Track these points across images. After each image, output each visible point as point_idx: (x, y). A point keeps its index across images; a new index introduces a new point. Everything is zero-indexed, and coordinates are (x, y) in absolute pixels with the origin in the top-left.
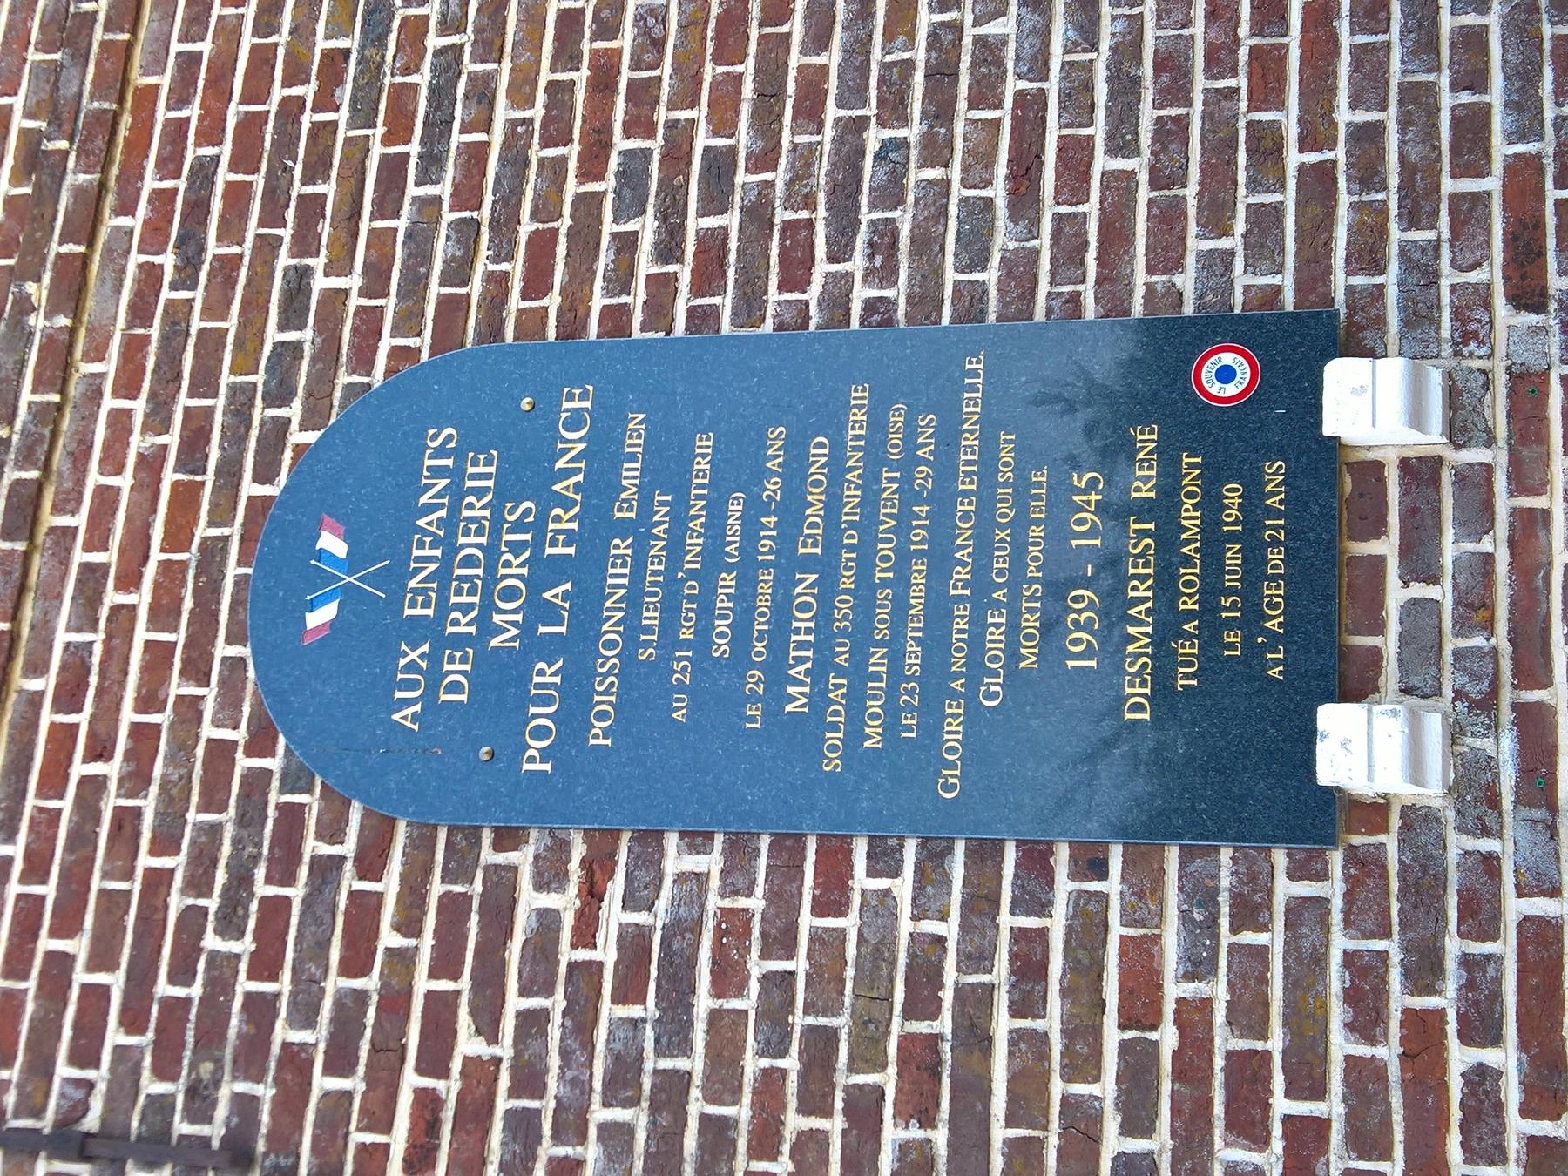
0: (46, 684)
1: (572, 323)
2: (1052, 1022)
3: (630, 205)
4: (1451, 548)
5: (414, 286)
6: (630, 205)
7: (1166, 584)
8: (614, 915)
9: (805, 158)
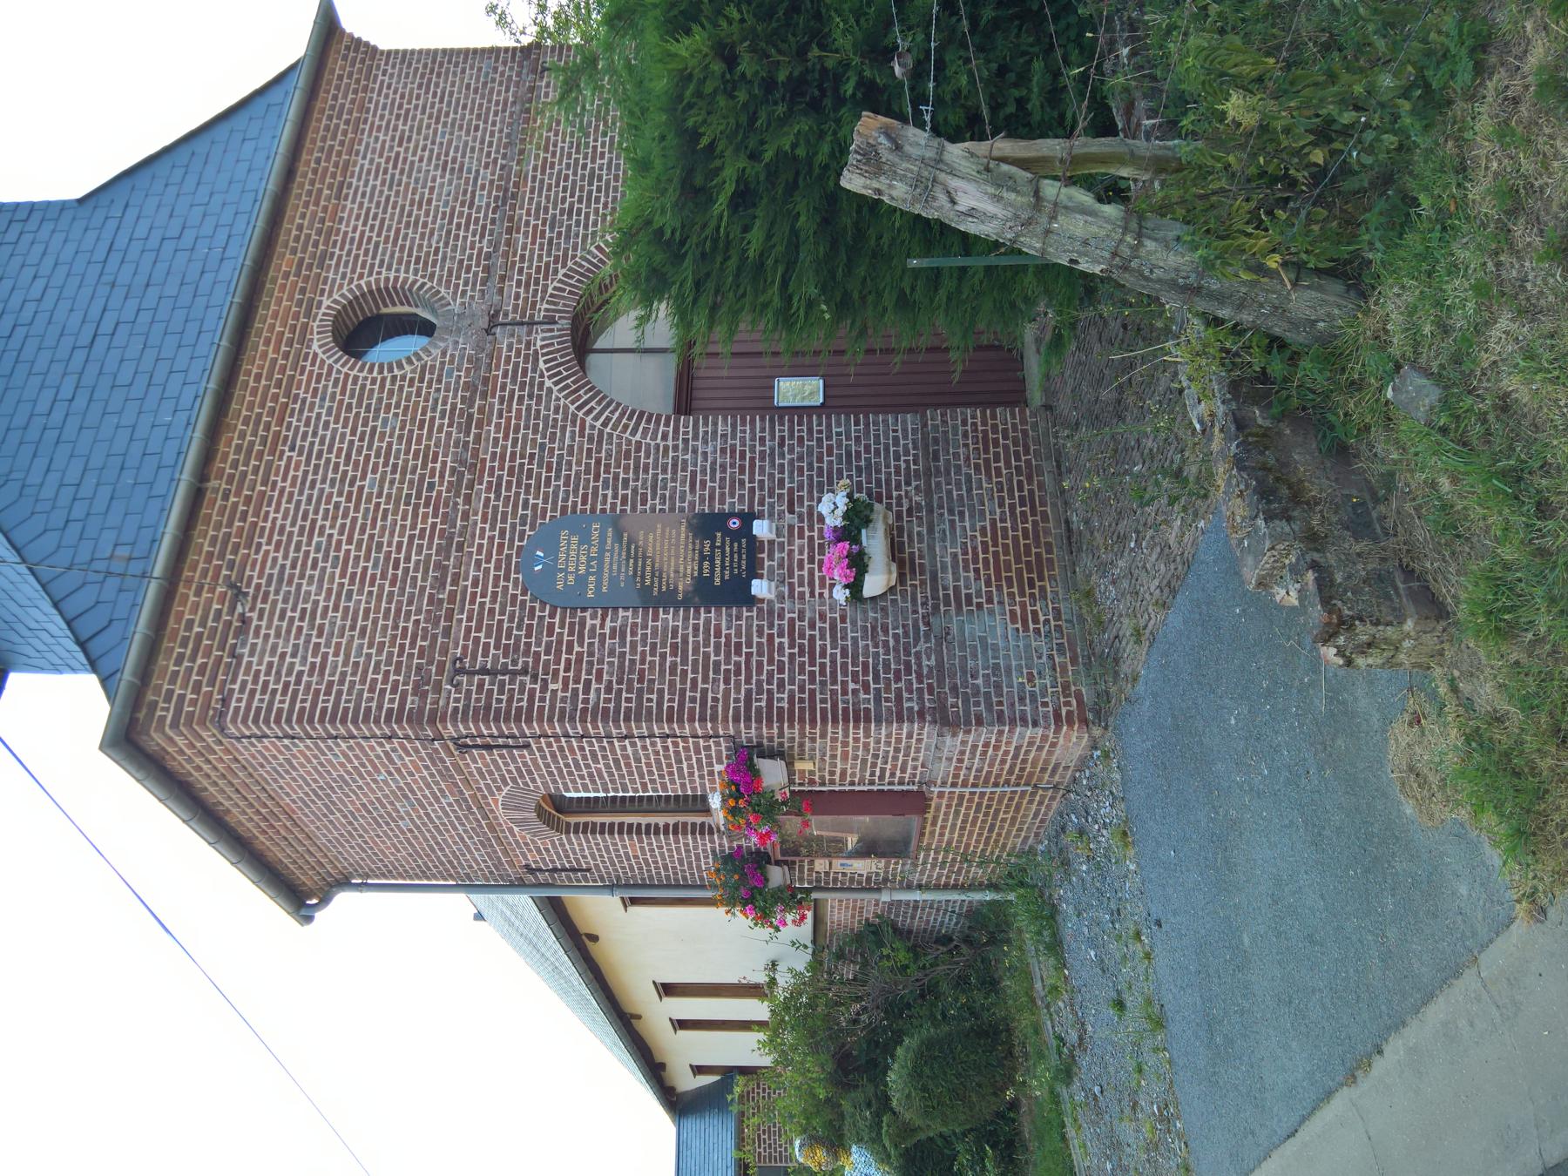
0: (469, 583)
1: (593, 510)
2: (701, 638)
3: (606, 487)
4: (777, 555)
5: (555, 503)
6: (606, 487)
7: (723, 562)
8: (608, 624)
9: (645, 481)
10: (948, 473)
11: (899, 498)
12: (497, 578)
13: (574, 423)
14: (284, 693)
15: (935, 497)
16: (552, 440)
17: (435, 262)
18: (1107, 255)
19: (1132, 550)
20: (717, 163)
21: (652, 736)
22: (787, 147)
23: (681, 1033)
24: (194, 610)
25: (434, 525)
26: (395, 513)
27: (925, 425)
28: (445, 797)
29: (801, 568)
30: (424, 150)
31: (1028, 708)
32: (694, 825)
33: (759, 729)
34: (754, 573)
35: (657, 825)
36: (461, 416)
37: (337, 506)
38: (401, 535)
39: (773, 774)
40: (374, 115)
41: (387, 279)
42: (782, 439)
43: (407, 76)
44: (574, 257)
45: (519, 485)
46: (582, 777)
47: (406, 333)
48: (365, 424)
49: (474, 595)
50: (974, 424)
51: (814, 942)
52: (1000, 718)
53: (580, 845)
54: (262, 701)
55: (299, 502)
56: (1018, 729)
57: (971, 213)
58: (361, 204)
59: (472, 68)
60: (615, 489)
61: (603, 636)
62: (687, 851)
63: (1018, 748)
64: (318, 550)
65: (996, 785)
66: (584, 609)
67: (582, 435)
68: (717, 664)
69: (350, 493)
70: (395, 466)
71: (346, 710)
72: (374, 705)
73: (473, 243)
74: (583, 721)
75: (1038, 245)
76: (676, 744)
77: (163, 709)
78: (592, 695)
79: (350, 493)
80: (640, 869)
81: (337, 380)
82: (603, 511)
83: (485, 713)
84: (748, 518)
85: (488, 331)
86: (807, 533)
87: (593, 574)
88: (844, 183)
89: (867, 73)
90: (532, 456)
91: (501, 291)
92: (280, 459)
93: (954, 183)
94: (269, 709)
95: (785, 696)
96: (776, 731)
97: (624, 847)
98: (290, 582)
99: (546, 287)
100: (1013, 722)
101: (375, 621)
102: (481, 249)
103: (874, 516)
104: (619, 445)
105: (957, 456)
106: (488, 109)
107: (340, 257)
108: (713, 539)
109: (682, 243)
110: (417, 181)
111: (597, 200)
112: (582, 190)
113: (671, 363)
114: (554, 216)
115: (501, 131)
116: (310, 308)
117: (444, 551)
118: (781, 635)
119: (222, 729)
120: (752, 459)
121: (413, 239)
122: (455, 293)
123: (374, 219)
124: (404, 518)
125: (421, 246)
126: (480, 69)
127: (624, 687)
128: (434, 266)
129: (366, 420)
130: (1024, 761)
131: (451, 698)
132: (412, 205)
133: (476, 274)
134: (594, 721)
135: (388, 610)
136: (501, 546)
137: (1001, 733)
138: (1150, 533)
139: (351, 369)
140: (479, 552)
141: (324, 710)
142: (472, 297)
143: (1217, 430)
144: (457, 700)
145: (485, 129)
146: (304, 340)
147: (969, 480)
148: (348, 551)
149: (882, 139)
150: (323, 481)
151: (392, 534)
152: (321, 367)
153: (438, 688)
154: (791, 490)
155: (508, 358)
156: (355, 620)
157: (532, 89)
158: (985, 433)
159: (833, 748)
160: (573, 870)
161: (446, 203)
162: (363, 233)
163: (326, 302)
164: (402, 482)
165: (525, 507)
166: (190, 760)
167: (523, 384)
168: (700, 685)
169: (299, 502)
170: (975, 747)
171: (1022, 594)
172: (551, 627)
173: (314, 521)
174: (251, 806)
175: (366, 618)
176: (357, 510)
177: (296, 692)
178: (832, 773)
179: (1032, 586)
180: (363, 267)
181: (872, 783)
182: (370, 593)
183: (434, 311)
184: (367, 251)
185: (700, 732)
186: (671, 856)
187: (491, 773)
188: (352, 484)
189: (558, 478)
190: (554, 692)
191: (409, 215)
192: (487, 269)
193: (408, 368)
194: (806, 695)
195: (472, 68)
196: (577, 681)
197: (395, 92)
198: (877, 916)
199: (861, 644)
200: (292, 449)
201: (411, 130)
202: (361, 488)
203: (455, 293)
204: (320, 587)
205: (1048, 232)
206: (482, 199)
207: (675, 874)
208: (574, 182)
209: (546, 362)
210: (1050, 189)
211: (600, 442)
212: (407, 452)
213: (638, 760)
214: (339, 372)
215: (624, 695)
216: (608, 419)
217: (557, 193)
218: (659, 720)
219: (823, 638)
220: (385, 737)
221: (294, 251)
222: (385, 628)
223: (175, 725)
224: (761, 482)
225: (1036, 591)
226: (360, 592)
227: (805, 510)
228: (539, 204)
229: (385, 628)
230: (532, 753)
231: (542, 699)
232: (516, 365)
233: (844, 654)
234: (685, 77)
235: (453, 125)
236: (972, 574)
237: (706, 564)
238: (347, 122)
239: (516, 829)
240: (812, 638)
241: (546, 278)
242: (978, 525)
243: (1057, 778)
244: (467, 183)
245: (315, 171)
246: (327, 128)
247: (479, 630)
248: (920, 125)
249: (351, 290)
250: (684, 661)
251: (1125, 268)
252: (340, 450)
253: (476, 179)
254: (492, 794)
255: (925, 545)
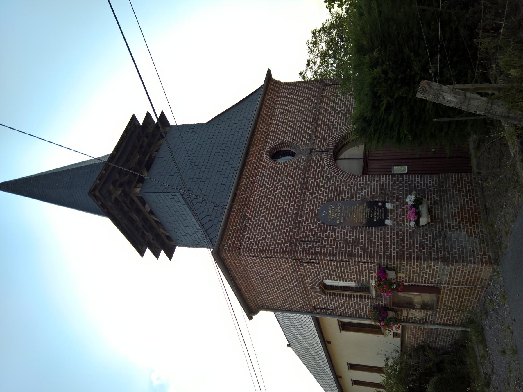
1: (339, 200)
2: (370, 235)
5: (328, 198)
10: (447, 191)
11: (431, 198)
12: (312, 217)
13: (333, 177)
14: (256, 244)
15: (442, 198)
16: (327, 182)
17: (296, 136)
18: (484, 109)
19: (505, 208)
20: (382, 99)
21: (355, 262)
22: (401, 94)
23: (355, 386)
24: (234, 223)
25: (295, 203)
26: (285, 200)
27: (439, 178)
28: (294, 279)
29: (400, 217)
30: (293, 107)
31: (472, 259)
32: (365, 296)
33: (387, 261)
34: (386, 217)
35: (354, 295)
36: (302, 175)
37: (270, 198)
38: (286, 206)
39: (391, 275)
40: (280, 99)
41: (283, 141)
42: (395, 181)
43: (289, 89)
44: (334, 134)
45: (318, 193)
46: (333, 275)
47: (287, 156)
48: (277, 177)
49: (305, 221)
50: (455, 178)
51: (401, 350)
52: (463, 261)
53: (331, 300)
54: (250, 246)
55: (260, 197)
56: (469, 265)
57: (449, 101)
58: (277, 122)
59: (306, 86)
60: (345, 195)
61: (341, 234)
62: (363, 305)
63: (469, 272)
64: (264, 209)
65: (462, 285)
66: (336, 226)
67: (336, 180)
68: (375, 242)
69: (273, 195)
70: (285, 188)
71: (271, 249)
72: (279, 249)
73: (306, 131)
74: (336, 256)
75: (466, 108)
76: (362, 265)
77: (226, 247)
78: (338, 249)
79: (273, 195)
80: (348, 310)
81: (270, 166)
82: (342, 200)
83: (308, 252)
84: (384, 203)
85: (310, 154)
86: (402, 207)
87: (338, 217)
88: (417, 96)
89: (423, 75)
90: (322, 186)
91: (314, 143)
92: (255, 186)
93: (444, 94)
94: (252, 248)
95: (396, 252)
96: (392, 262)
97: (344, 302)
98: (257, 217)
99: (326, 142)
100: (467, 262)
101: (279, 227)
102: (308, 132)
103: (423, 202)
104: (346, 183)
105: (449, 186)
106: (311, 96)
107: (271, 135)
108: (374, 208)
109: (371, 120)
110: (291, 115)
111: (341, 119)
112: (337, 116)
113: (362, 161)
114: (329, 123)
115: (314, 102)
116: (263, 148)
117: (298, 210)
118: (394, 235)
119: (240, 253)
120: (386, 187)
121: (290, 131)
122: (301, 144)
123: (280, 126)
124: (287, 201)
125: (292, 132)
126: (309, 86)
127: (347, 247)
128: (296, 137)
129: (277, 177)
130: (471, 277)
131: (300, 248)
132: (290, 122)
133: (307, 139)
134: (339, 256)
135: (282, 225)
136: (313, 209)
137: (463, 266)
138: (510, 201)
139: (274, 164)
140: (307, 210)
141: (266, 249)
142: (306, 145)
143: (517, 154)
144: (301, 248)
145: (310, 101)
146: (262, 157)
147: (453, 193)
148: (272, 210)
149: (427, 85)
150: (266, 192)
151: (284, 205)
152: (266, 163)
153: (296, 245)
154: (397, 196)
155: (315, 161)
156: (274, 227)
157: (323, 91)
158: (458, 180)
159: (410, 269)
160: (328, 309)
161: (299, 121)
162: (277, 129)
163: (267, 147)
164: (287, 192)
165: (320, 199)
166: (230, 262)
167: (319, 167)
168: (370, 248)
169: (260, 197)
170: (455, 271)
171: (470, 226)
172: (327, 231)
173: (264, 202)
174: (242, 278)
175: (277, 226)
176: (275, 199)
177: (258, 244)
178: (409, 278)
179: (474, 223)
180: (277, 138)
181: (422, 283)
182: (278, 220)
183: (296, 150)
184: (278, 134)
185: (369, 261)
186: (358, 306)
187: (308, 272)
188: (273, 192)
189: (329, 191)
190: (327, 248)
191: (289, 124)
192: (310, 138)
193: (288, 163)
194: (402, 252)
195: (306, 86)
196: (334, 245)
197: (286, 93)
198: (423, 342)
199: (419, 239)
200: (258, 184)
201: (290, 103)
202: (276, 194)
203: (301, 144)
204: (265, 218)
205: (468, 105)
206: (309, 120)
207: (358, 313)
208: (335, 114)
209: (326, 161)
210: (468, 94)
211: (341, 182)
212: (288, 185)
213: (350, 270)
214: (270, 164)
215: (347, 249)
216: (343, 176)
217: (330, 117)
218: (358, 257)
219: (407, 236)
220: (282, 258)
221: (259, 134)
222: (282, 229)
223: (228, 251)
224: (388, 193)
225: (475, 225)
226: (275, 220)
227: (402, 201)
228: (324, 120)
229: (282, 229)
230: (320, 266)
231: (324, 249)
232: (318, 162)
233: (414, 241)
234: (374, 79)
235: (301, 101)
236: (454, 220)
237: (372, 215)
238: (273, 101)
239: (313, 292)
240: (404, 237)
241: (326, 140)
242: (456, 206)
243: (483, 284)
244: (305, 115)
245: (265, 114)
246: (268, 103)
247: (307, 231)
248: (436, 81)
249: (274, 144)
250: (365, 241)
251: (489, 113)
252: (271, 184)
253: (307, 114)
254: (307, 279)
255: (439, 212)
